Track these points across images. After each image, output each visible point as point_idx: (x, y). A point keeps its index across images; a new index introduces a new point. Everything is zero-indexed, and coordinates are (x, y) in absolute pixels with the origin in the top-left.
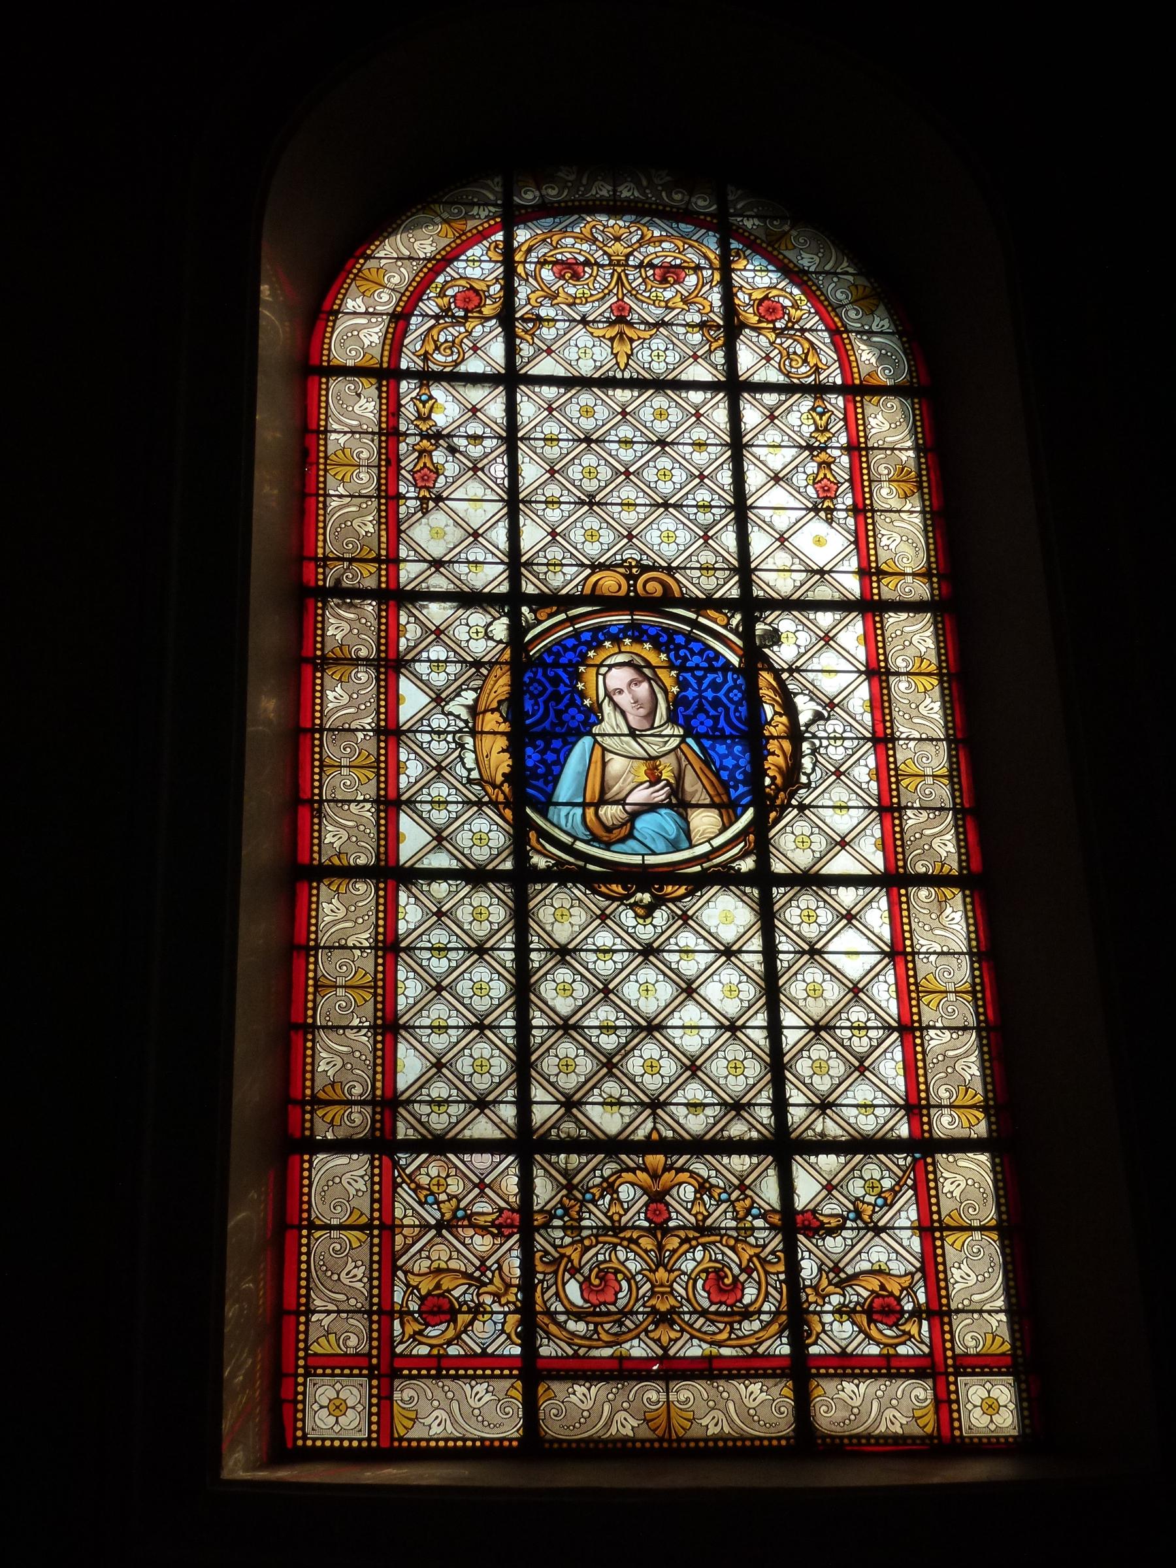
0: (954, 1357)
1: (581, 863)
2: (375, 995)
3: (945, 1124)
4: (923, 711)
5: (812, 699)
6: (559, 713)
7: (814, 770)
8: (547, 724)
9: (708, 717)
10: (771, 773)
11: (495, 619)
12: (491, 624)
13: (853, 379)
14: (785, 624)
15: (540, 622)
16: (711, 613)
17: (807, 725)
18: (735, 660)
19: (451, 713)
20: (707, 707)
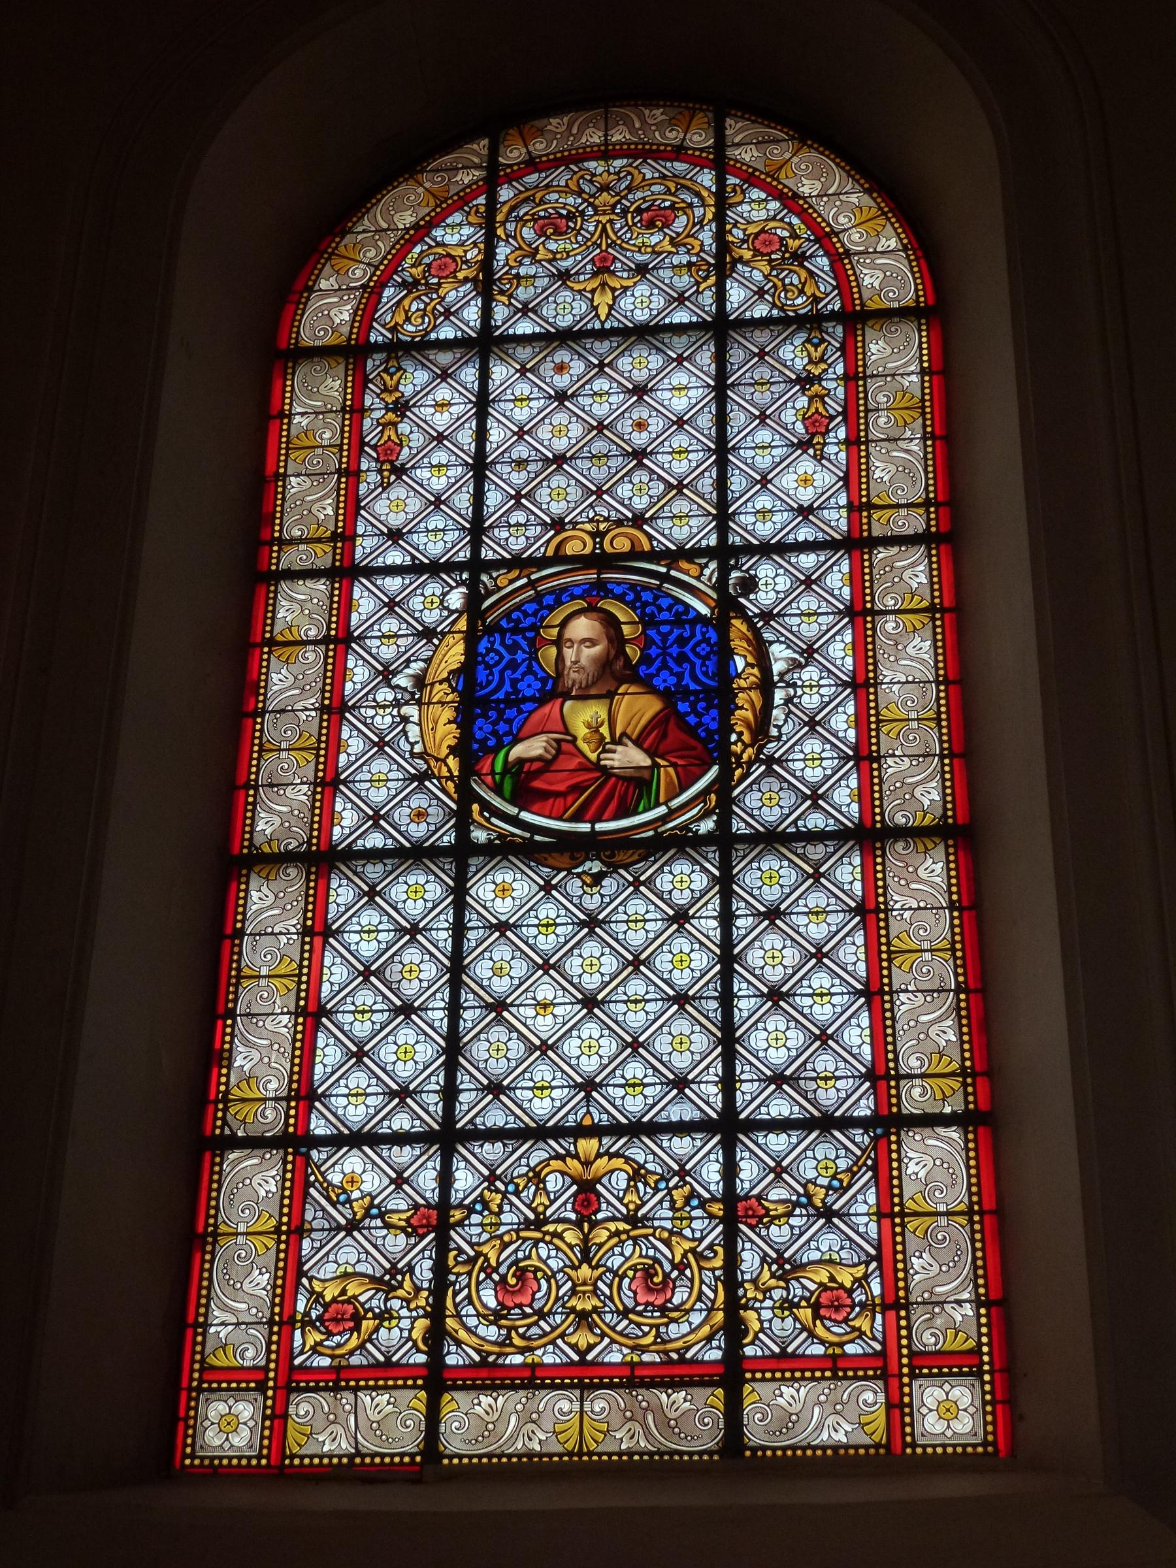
0: (912, 1355)
1: (528, 835)
2: (318, 756)
3: (915, 1098)
4: (911, 660)
5: (789, 647)
6: (514, 682)
7: (786, 721)
8: (501, 695)
9: (672, 674)
10: (738, 729)
11: (452, 588)
12: (448, 593)
13: (862, 531)
14: (764, 570)
15: (500, 589)
16: (684, 565)
17: (782, 675)
18: (704, 610)
19: (398, 686)
20: (671, 663)
